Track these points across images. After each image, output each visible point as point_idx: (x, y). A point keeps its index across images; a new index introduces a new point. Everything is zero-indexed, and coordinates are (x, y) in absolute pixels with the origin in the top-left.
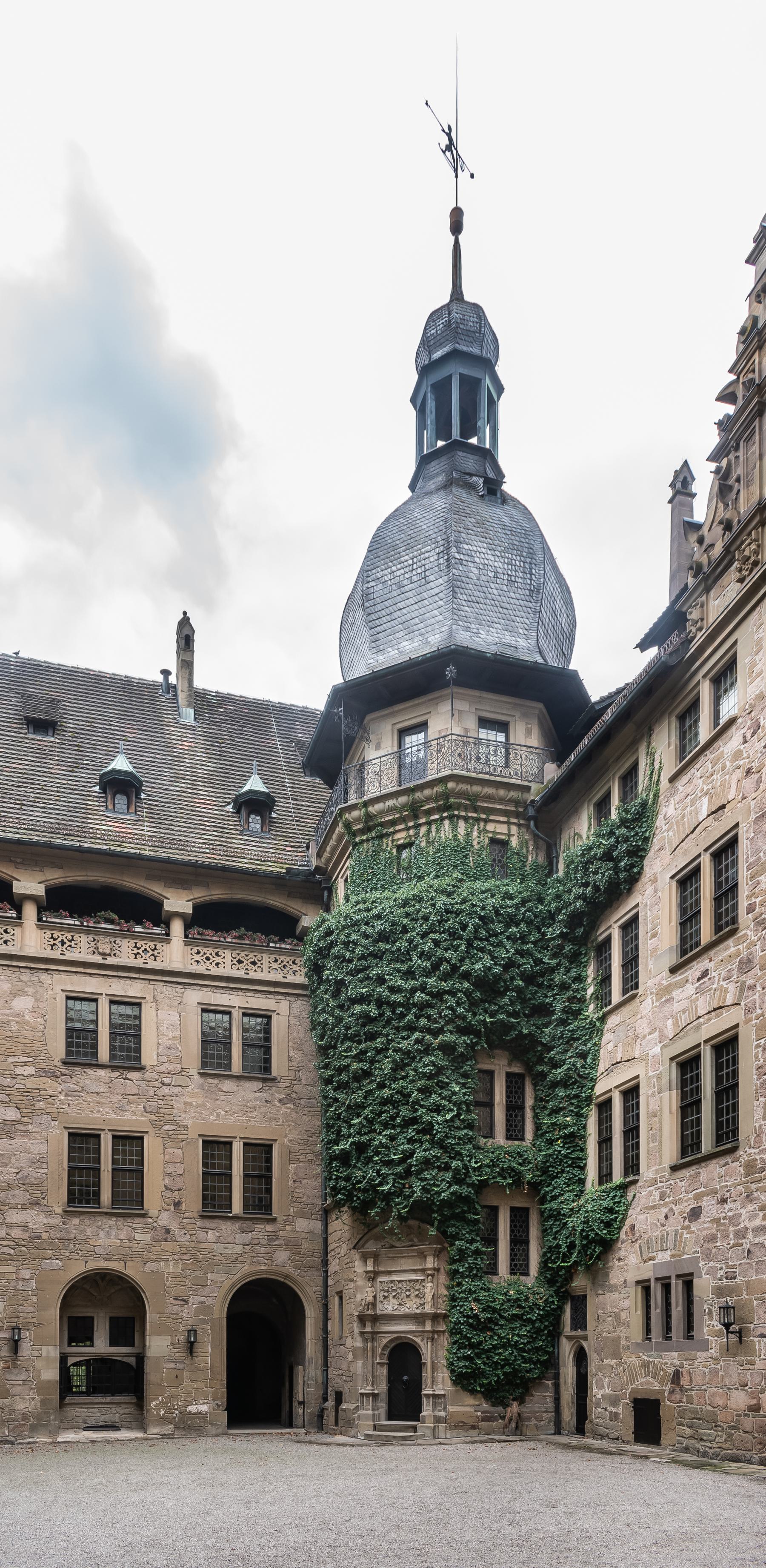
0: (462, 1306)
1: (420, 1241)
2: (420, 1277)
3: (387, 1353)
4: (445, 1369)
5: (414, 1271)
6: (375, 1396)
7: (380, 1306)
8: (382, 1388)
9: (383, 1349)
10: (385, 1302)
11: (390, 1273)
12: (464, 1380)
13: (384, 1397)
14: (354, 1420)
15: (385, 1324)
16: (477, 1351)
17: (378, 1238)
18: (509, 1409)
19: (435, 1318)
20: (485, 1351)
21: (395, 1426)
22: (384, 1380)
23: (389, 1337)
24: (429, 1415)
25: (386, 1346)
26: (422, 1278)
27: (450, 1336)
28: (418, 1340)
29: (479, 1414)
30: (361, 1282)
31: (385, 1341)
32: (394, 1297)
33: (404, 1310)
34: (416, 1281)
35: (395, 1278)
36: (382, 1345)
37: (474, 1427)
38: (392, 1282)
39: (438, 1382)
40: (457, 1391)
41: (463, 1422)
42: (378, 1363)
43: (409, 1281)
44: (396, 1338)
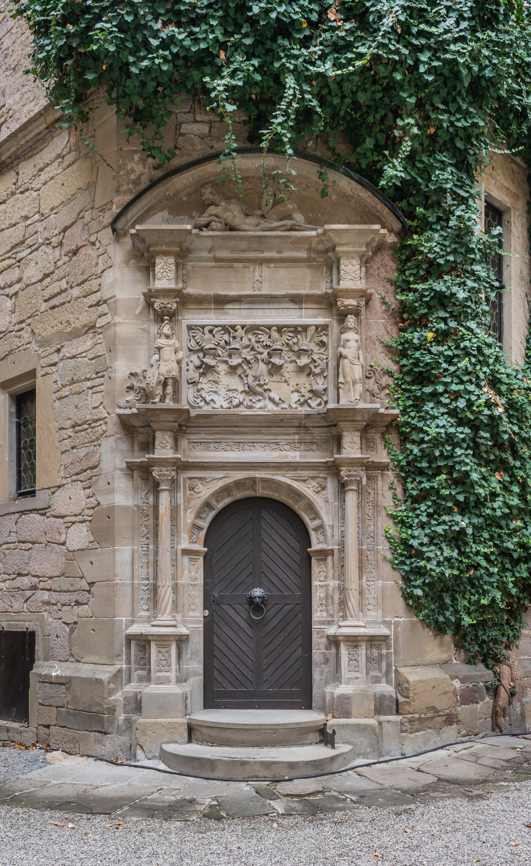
0: (457, 395)
1: (309, 221)
2: (312, 317)
3: (205, 524)
4: (387, 568)
5: (297, 300)
6: (181, 641)
7: (188, 394)
8: (189, 619)
9: (198, 516)
10: (205, 384)
11: (221, 302)
12: (434, 600)
13: (197, 643)
14: (112, 710)
15: (205, 444)
16: (475, 521)
17: (193, 204)
18: (505, 669)
19: (372, 426)
20: (492, 522)
21: (274, 728)
22: (196, 596)
23: (219, 480)
24: (364, 694)
25: (207, 505)
26: (320, 321)
27: (404, 481)
28: (307, 490)
29: (457, 684)
30: (127, 325)
31: (205, 492)
32: (233, 369)
33: (263, 407)
34: (299, 330)
35: (234, 316)
36: (197, 503)
37: (450, 719)
38: (227, 329)
39: (359, 600)
40: (413, 624)
41: (433, 708)
42: (185, 552)
43: (280, 329)
44: (239, 484)
